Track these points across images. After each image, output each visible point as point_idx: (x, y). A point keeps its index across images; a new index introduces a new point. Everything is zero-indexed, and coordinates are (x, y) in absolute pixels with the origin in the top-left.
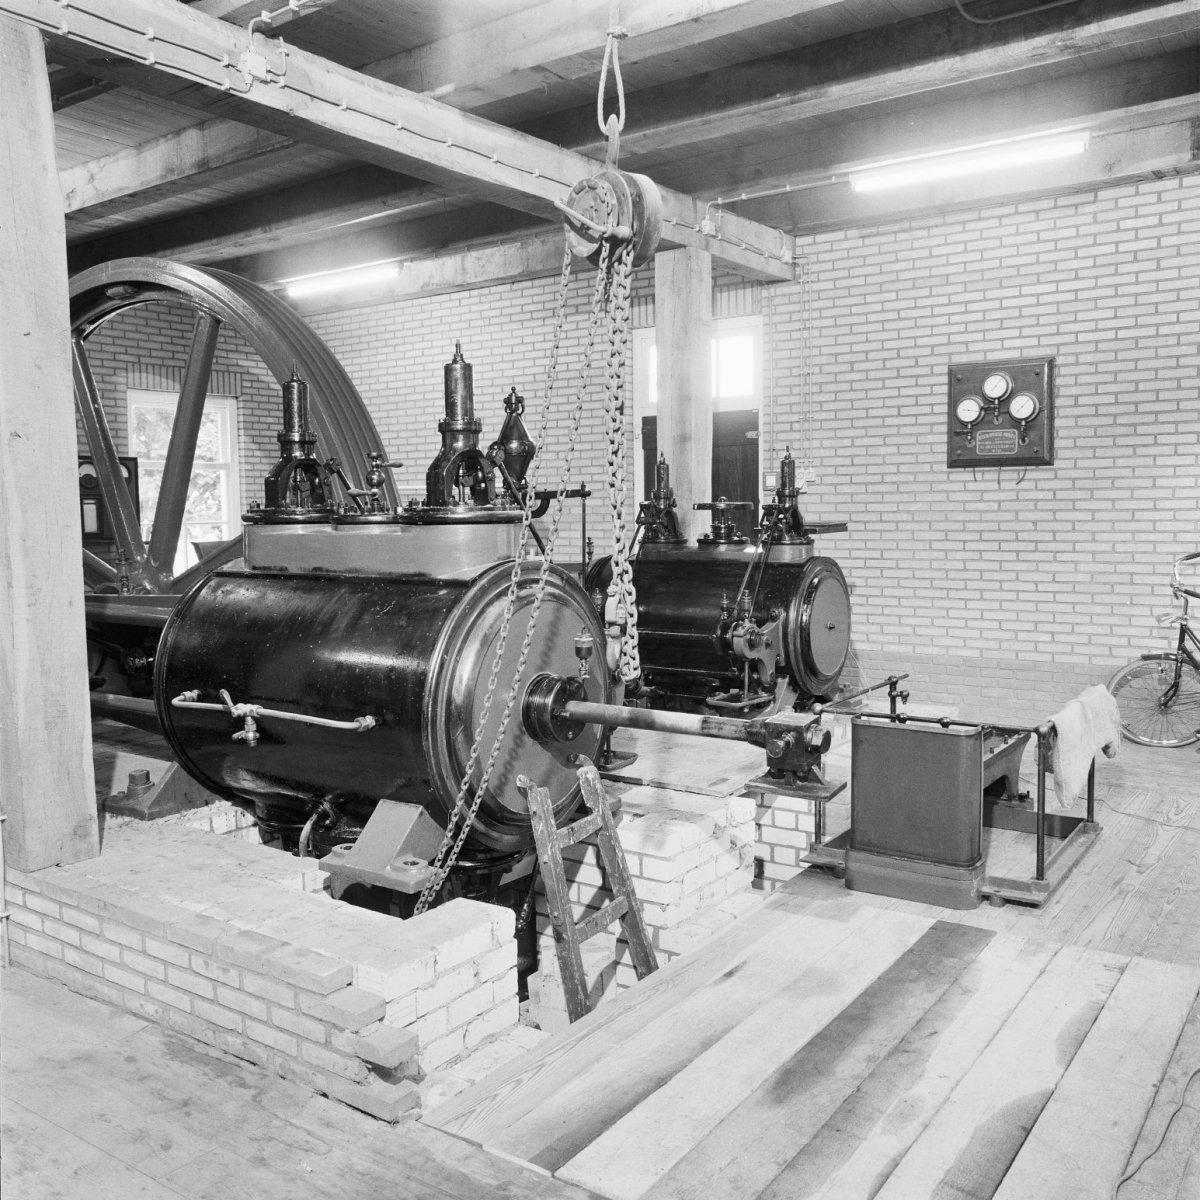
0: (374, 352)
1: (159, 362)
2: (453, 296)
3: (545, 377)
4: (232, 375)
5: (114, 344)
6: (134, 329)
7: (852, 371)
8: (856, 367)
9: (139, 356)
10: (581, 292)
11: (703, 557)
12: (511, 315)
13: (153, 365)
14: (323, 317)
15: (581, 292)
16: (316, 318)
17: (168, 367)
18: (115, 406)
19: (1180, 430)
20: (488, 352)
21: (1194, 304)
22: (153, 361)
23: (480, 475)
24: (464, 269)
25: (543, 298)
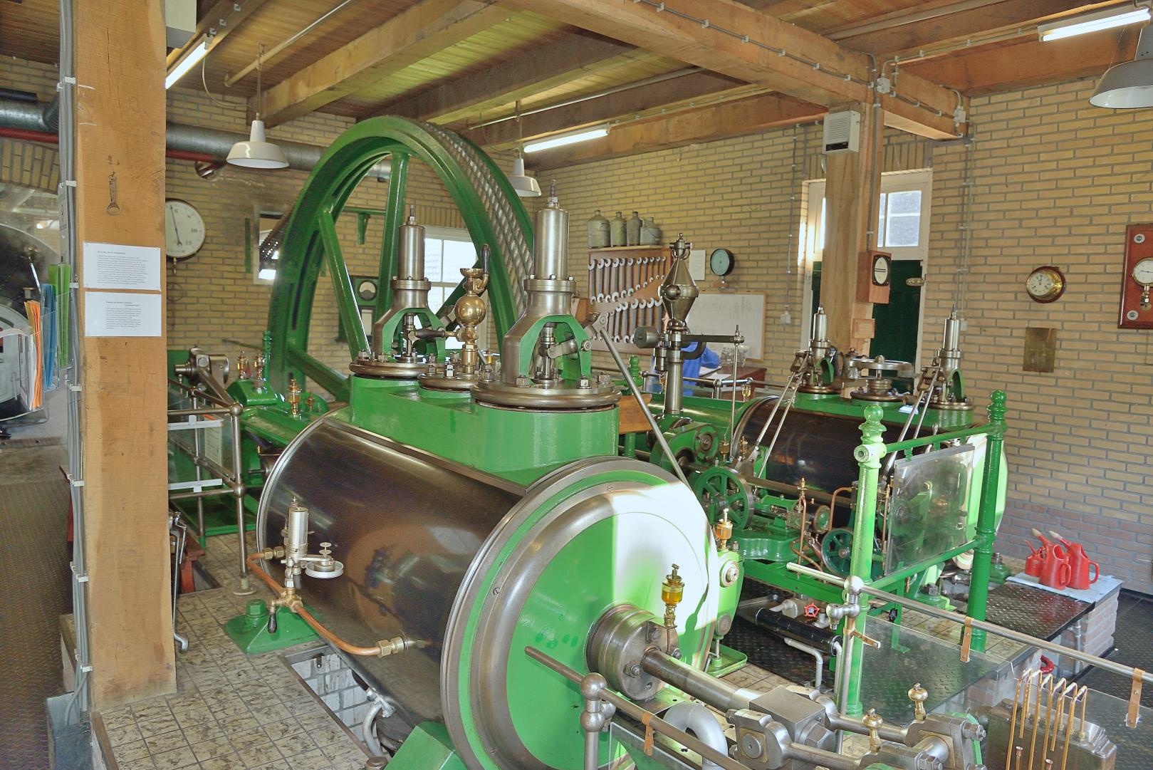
1: (431, 204)
15: (766, 150)
17: (436, 208)
22: (426, 204)
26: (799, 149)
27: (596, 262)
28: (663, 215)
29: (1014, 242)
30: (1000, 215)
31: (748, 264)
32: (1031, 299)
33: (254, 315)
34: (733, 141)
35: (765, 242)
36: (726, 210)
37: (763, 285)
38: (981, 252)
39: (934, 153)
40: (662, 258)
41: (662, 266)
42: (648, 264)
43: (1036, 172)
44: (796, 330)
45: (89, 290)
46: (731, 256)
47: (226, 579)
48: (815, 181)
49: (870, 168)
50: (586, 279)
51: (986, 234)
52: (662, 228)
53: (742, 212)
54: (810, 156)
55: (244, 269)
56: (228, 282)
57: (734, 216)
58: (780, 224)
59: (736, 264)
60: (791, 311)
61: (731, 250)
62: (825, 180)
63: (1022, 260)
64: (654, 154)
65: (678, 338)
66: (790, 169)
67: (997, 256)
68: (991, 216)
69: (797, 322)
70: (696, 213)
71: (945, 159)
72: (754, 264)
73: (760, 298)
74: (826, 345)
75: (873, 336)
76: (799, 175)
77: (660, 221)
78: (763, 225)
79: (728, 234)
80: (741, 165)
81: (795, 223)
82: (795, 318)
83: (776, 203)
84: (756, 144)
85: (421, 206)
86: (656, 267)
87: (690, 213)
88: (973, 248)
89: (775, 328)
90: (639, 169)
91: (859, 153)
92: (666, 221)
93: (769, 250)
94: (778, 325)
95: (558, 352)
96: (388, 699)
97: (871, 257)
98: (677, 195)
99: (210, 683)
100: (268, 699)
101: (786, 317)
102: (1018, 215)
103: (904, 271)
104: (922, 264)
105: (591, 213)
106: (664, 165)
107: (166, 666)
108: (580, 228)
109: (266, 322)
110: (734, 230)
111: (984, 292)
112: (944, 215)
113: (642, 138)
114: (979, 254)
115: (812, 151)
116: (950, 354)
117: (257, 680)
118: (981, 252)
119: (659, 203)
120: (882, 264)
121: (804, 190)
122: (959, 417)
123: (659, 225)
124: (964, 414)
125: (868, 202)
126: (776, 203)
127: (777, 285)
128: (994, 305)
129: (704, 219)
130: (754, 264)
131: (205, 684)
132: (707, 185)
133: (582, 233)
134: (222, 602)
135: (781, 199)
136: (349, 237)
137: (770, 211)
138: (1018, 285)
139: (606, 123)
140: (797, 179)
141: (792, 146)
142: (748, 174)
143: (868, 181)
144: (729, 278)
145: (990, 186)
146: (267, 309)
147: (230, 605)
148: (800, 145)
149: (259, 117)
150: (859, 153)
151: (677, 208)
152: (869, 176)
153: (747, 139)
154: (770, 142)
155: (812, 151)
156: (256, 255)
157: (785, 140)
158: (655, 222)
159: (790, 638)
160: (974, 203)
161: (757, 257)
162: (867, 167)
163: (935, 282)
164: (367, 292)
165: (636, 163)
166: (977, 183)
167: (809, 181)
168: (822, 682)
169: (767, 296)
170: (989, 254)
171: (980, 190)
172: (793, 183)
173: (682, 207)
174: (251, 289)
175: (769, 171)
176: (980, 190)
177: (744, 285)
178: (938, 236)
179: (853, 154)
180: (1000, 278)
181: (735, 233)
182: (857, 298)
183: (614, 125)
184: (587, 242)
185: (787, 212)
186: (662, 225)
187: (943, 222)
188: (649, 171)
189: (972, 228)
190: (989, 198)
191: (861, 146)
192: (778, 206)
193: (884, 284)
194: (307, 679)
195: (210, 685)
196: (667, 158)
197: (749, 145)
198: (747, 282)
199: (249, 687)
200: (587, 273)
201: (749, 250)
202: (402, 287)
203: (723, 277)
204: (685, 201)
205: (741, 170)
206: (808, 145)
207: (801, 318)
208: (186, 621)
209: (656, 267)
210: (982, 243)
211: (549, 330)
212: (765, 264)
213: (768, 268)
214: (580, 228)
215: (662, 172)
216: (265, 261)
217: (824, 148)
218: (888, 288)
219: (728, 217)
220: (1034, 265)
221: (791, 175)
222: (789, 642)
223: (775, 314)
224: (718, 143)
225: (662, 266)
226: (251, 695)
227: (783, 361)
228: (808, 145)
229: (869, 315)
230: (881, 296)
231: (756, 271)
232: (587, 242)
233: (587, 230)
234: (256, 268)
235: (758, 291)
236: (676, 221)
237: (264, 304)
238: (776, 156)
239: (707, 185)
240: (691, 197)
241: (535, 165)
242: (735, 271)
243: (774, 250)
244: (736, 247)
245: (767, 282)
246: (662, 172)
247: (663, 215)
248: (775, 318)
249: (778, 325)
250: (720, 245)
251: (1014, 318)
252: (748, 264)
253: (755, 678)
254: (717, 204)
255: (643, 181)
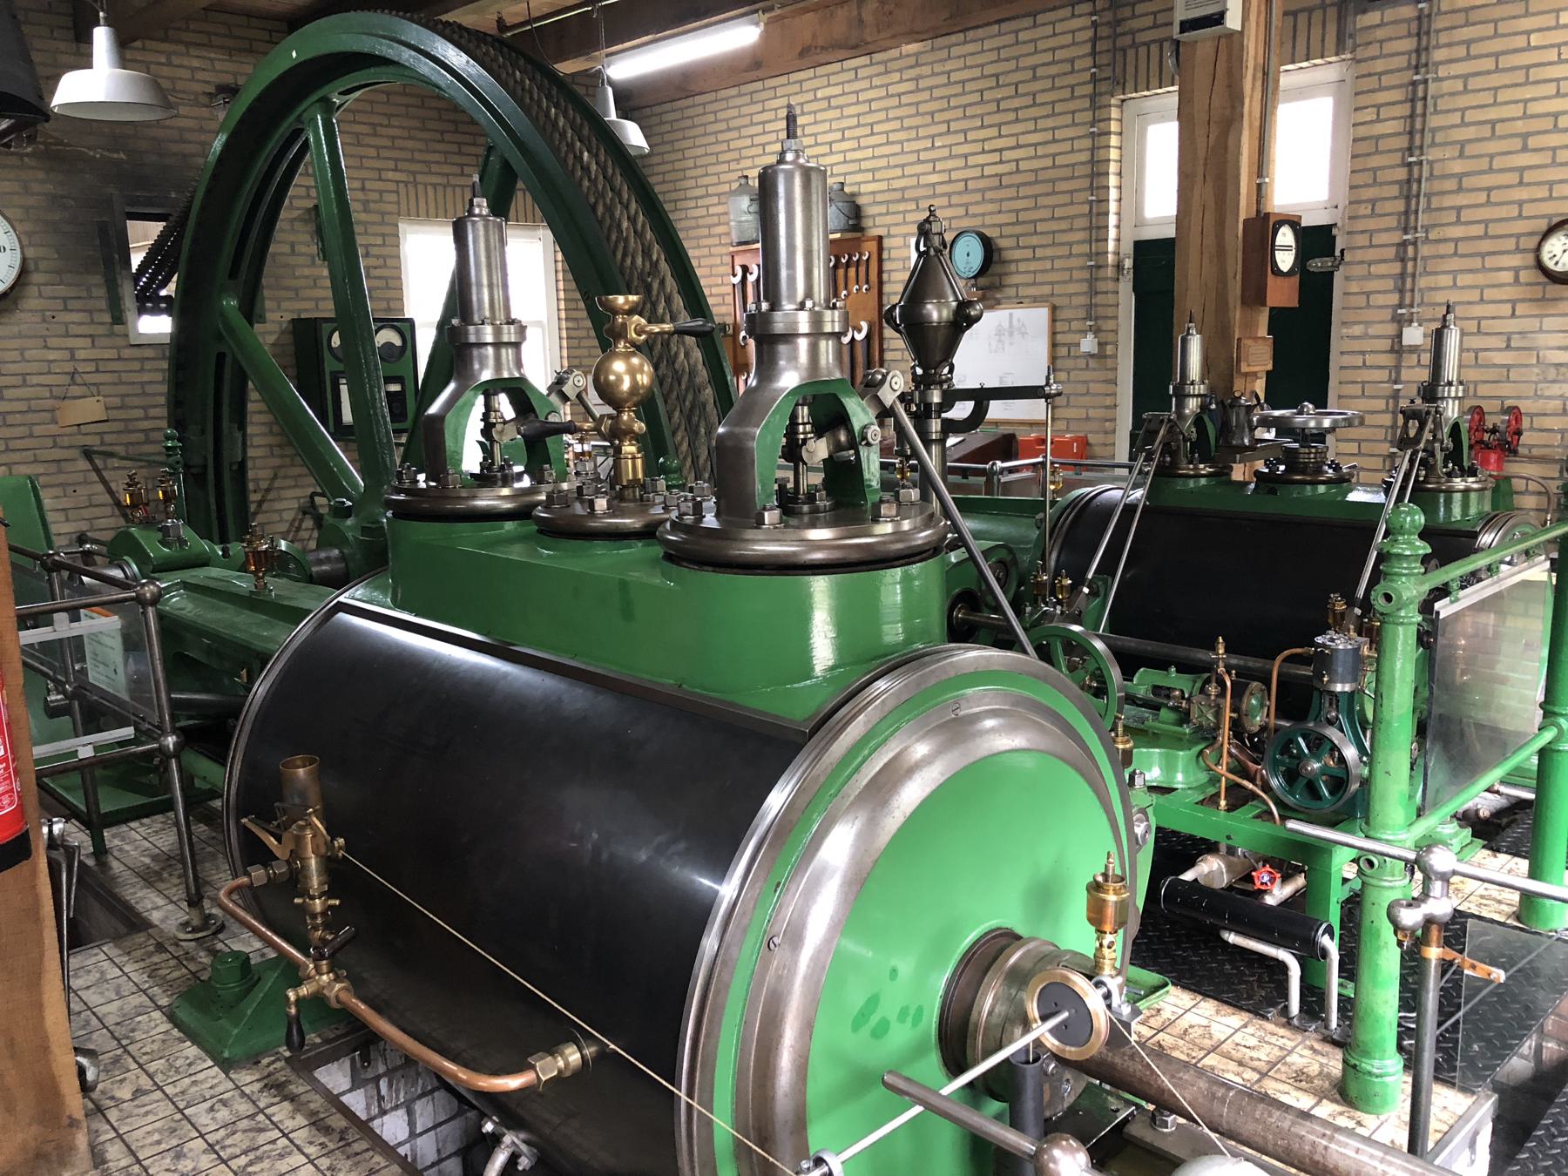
0: (735, 155)
1: (444, 181)
2: (847, 64)
3: (1088, 62)
4: (420, 187)
5: (378, 157)
6: (406, 134)
7: (1525, 149)
8: (1532, 142)
9: (414, 173)
10: (1041, 45)
11: (1271, 506)
12: (931, 88)
13: (434, 186)
14: (667, 107)
15: (1041, 45)
16: (657, 109)
17: (454, 186)
18: (384, 245)
19: (1490, 233)
20: (897, 148)
21: (8, 393)
22: (435, 179)
23: (843, 438)
24: (861, 21)
25: (980, 59)
26: (1102, 38)
27: (745, 269)
28: (859, 178)
29: (1513, 178)
30: (1486, 131)
31: (1017, 254)
32: (1543, 279)
33: (136, 401)
34: (980, 32)
35: (1046, 214)
36: (972, 161)
37: (1047, 290)
38: (1448, 201)
39: (1358, 26)
40: (861, 255)
41: (862, 269)
42: (848, 264)
43: (1552, 46)
44: (1109, 363)
45: (1396, 198)
46: (987, 243)
47: (157, 908)
48: (1134, 95)
49: (1261, 61)
50: (729, 299)
51: (1457, 167)
52: (861, 201)
53: (1001, 162)
54: (1124, 50)
55: (107, 318)
56: (79, 342)
57: (988, 171)
58: (1073, 178)
59: (995, 258)
60: (1097, 331)
61: (988, 232)
62: (1176, 88)
63: (1528, 210)
64: (836, 67)
65: (936, 397)
66: (1087, 76)
67: (1481, 205)
68: (1470, 133)
69: (1109, 350)
70: (919, 169)
71: (1380, 34)
72: (1028, 253)
73: (1041, 315)
74: (1202, 389)
75: (1270, 367)
76: (1103, 87)
77: (855, 189)
78: (1043, 181)
79: (977, 203)
80: (997, 76)
81: (1099, 174)
82: (1106, 344)
83: (1064, 140)
84: (1022, 36)
85: (426, 185)
86: (852, 271)
87: (909, 170)
88: (1434, 194)
89: (1069, 363)
90: (810, 96)
91: (1241, 33)
92: (864, 189)
93: (1054, 226)
94: (1077, 357)
95: (819, 450)
96: (523, 1136)
97: (1263, 227)
98: (883, 139)
99: (156, 1137)
100: (281, 1156)
101: (1088, 344)
102: (1520, 126)
103: (1316, 241)
104: (1335, 231)
105: (729, 182)
106: (856, 86)
107: (67, 1121)
108: (712, 210)
109: (164, 412)
110: (989, 195)
111: (1454, 273)
112: (1378, 138)
113: (814, 37)
114: (1445, 205)
115: (1127, 40)
116: (1444, 391)
117: (252, 1117)
118: (1448, 201)
119: (850, 156)
120: (1285, 237)
121: (1114, 113)
122: (1465, 506)
123: (853, 195)
124: (1473, 496)
125: (1257, 124)
126: (1064, 140)
127: (1072, 288)
128: (1475, 295)
129: (934, 178)
130: (1028, 253)
131: (150, 1140)
132: (937, 117)
133: (715, 220)
134: (156, 959)
135: (1070, 133)
136: (303, 249)
137: (1054, 156)
138: (1519, 256)
139: (756, 11)
140: (1101, 94)
141: (1090, 33)
142: (1011, 91)
143: (1259, 83)
144: (982, 281)
145: (1465, 77)
146: (164, 388)
147: (173, 962)
148: (1104, 31)
149: (105, 18)
150: (1241, 33)
151: (883, 162)
152: (1260, 75)
153: (1005, 26)
154: (1048, 30)
155: (1127, 40)
156: (128, 293)
157: (1076, 23)
158: (847, 189)
159: (1231, 930)
160: (1436, 112)
161: (1035, 240)
162: (1255, 58)
163: (1362, 262)
164: (389, 345)
165: (806, 86)
166: (1440, 75)
167: (1122, 97)
168: (1301, 1010)
169: (1054, 309)
170: (1465, 202)
171: (1447, 86)
172: (1093, 101)
173: (893, 161)
174: (127, 353)
175: (1048, 84)
176: (1447, 86)
177: (1011, 292)
178: (1366, 178)
179: (1231, 34)
180: (1485, 246)
181: (992, 201)
182: (1243, 303)
183: (773, 14)
184: (728, 234)
185: (1085, 157)
186: (859, 194)
187: (1377, 152)
188: (829, 98)
189: (1430, 158)
190: (1463, 101)
191: (1245, 19)
192: (1067, 146)
193: (1291, 273)
194: (344, 1093)
195: (159, 1143)
196: (862, 73)
197: (1010, 39)
198: (1017, 286)
199: (238, 1136)
200: (730, 289)
201: (1018, 229)
202: (472, 339)
203: (973, 281)
204: (897, 148)
205: (998, 86)
206: (1119, 30)
207: (1116, 344)
208: (89, 1009)
209: (852, 271)
210: (1451, 185)
211: (804, 412)
212: (1049, 252)
213: (1052, 259)
214: (712, 210)
215: (853, 98)
216: (148, 302)
217: (1177, 28)
218: (1296, 279)
219: (913, 182)
220: (1550, 217)
221: (1088, 89)
222: (1232, 938)
223: (1068, 338)
224: (954, 38)
225: (862, 269)
226: (245, 1153)
227: (1088, 418)
228: (1119, 30)
229: (1263, 331)
230: (1282, 294)
231: (1033, 266)
232: (728, 234)
233: (726, 213)
234: (130, 315)
235: (1036, 301)
236: (883, 186)
237: (156, 379)
238: (1060, 55)
239: (937, 117)
240: (908, 140)
241: (632, 100)
242: (995, 269)
243: (1064, 225)
244: (995, 225)
245: (1052, 283)
246: (853, 98)
247: (859, 178)
248: (1069, 345)
249: (1077, 357)
250: (966, 223)
251: (1513, 315)
252: (1017, 254)
253: (1175, 1009)
254: (957, 150)
255: (820, 116)
